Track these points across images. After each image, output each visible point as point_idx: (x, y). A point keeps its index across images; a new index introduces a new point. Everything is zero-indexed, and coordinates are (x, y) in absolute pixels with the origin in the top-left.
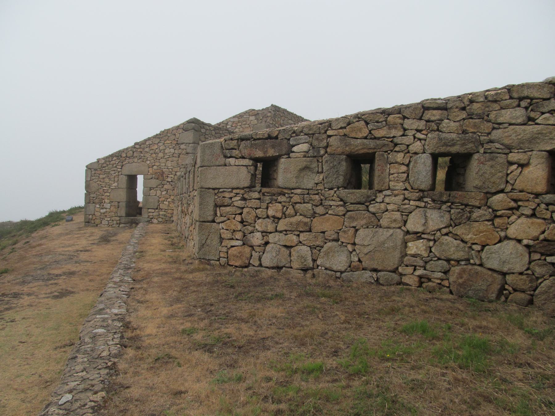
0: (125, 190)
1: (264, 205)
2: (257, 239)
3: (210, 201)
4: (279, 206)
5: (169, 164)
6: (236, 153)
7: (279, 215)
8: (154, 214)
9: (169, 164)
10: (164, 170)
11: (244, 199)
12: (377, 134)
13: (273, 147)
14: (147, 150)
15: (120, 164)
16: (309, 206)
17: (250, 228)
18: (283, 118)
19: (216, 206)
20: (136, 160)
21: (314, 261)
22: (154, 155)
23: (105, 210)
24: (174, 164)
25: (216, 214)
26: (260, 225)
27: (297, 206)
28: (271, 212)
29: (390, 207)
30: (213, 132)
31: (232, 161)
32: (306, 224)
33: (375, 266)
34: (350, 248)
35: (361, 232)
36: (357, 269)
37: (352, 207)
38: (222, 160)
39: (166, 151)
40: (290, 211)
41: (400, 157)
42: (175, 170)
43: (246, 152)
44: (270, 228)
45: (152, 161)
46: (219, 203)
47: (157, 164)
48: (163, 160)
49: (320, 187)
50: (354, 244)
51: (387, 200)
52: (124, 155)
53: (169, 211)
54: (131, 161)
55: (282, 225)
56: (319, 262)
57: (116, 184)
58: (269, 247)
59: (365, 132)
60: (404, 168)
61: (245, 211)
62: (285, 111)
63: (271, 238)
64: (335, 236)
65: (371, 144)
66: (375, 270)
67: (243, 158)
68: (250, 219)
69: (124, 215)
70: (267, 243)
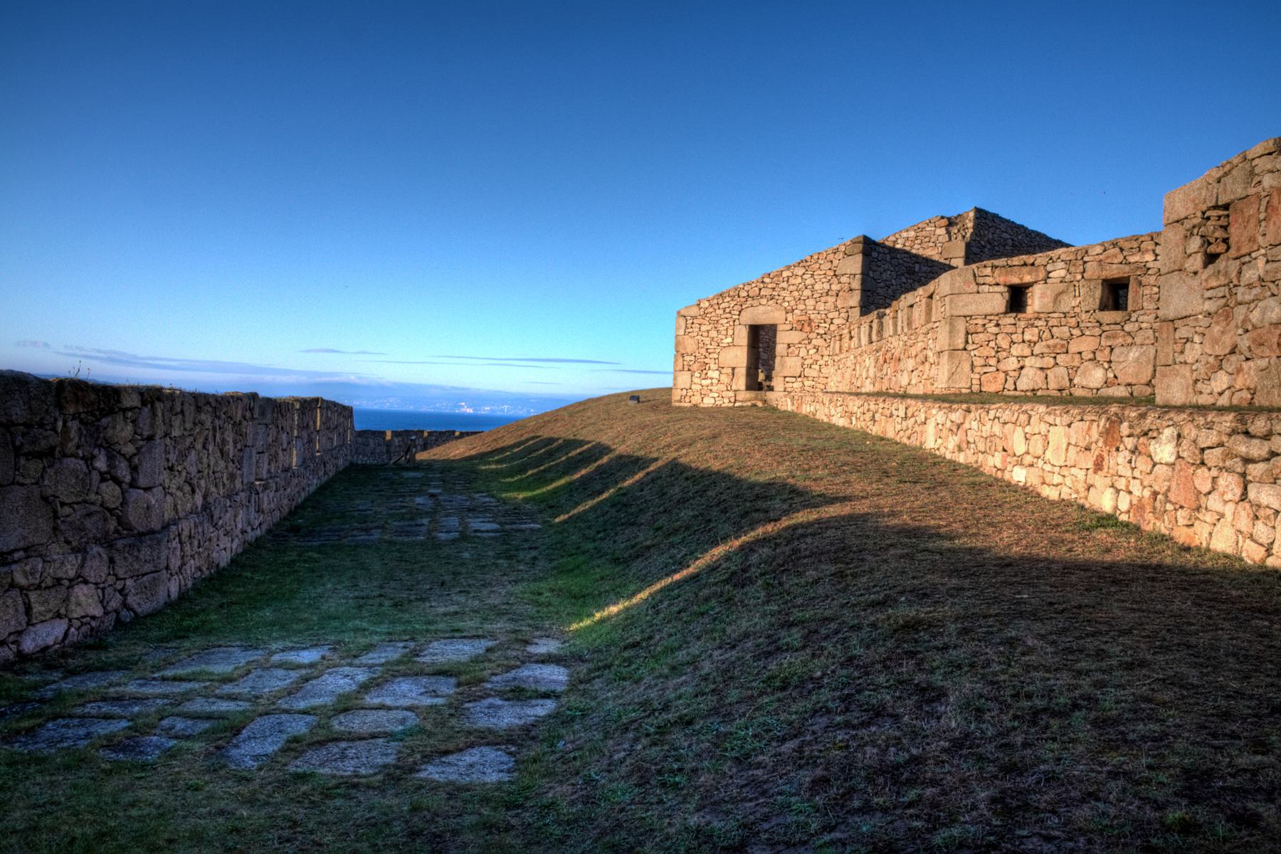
0: (745, 349)
1: (1020, 330)
2: (1012, 364)
3: (961, 326)
4: (1036, 330)
5: (821, 306)
6: (988, 280)
7: (1035, 339)
8: (795, 385)
9: (821, 306)
10: (812, 317)
11: (998, 325)
12: (1132, 259)
13: (1030, 273)
14: (785, 285)
15: (737, 307)
16: (1066, 329)
17: (1005, 354)
18: (992, 230)
19: (967, 333)
20: (764, 301)
21: (1071, 380)
22: (796, 294)
23: (709, 381)
24: (830, 305)
25: (967, 342)
26: (1016, 350)
27: (1054, 330)
28: (1027, 337)
29: (1144, 325)
30: (888, 257)
31: (986, 288)
32: (1063, 346)
33: (1130, 381)
34: (1106, 365)
35: (1116, 351)
36: (1113, 384)
37: (1106, 328)
38: (974, 287)
39: (817, 287)
40: (1046, 335)
41: (1152, 280)
42: (830, 316)
43: (1001, 280)
44: (1027, 352)
45: (793, 303)
46: (972, 330)
47: (802, 307)
48: (811, 302)
49: (1077, 310)
50: (1110, 362)
51: (1140, 319)
52: (744, 294)
53: (822, 380)
54: (755, 303)
55: (1037, 350)
56: (1075, 381)
57: (729, 340)
58: (1023, 372)
59: (1120, 258)
60: (1156, 290)
61: (999, 337)
62: (995, 216)
63: (1027, 362)
64: (1091, 356)
65: (1127, 268)
66: (1129, 385)
67: (998, 284)
68: (1005, 344)
69: (743, 387)
70: (1022, 368)
